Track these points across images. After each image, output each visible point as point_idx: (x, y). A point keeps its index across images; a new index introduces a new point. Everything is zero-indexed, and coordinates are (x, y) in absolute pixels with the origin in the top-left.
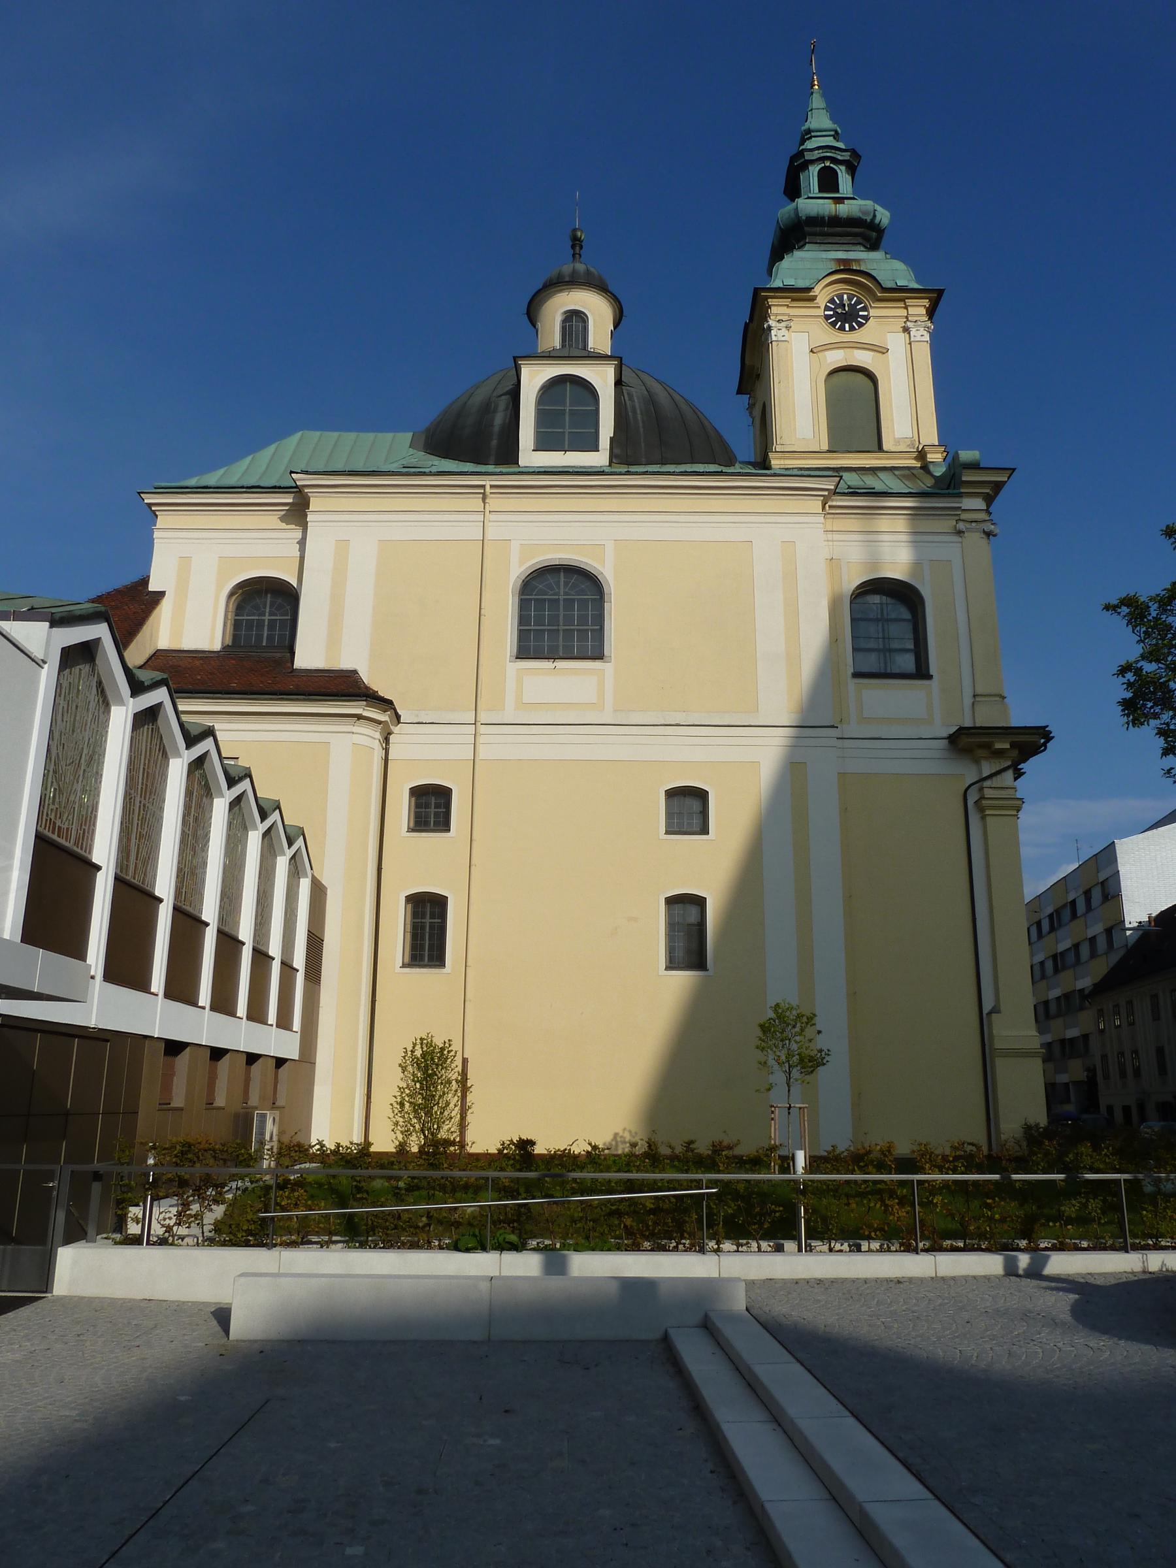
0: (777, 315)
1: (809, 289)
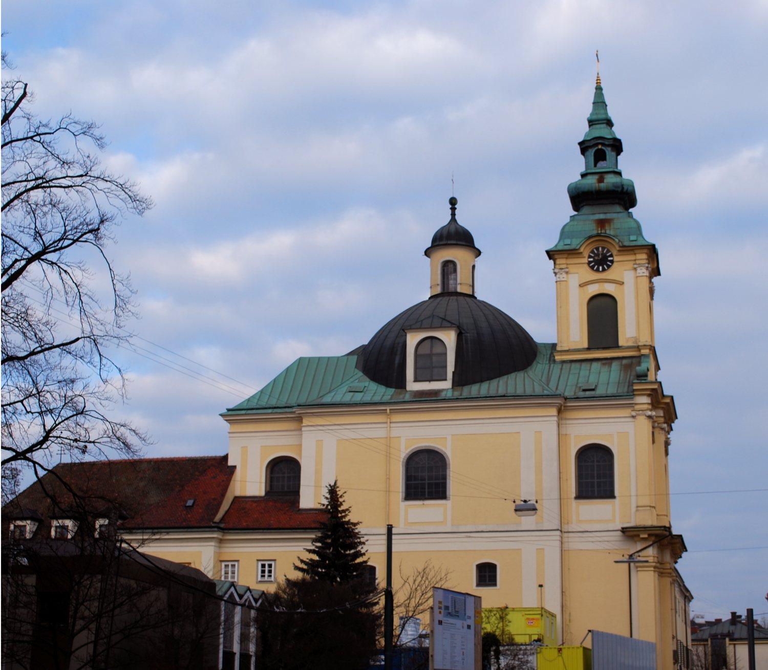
0: (560, 264)
1: (579, 249)
